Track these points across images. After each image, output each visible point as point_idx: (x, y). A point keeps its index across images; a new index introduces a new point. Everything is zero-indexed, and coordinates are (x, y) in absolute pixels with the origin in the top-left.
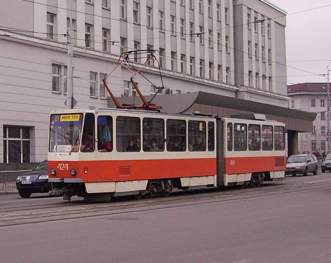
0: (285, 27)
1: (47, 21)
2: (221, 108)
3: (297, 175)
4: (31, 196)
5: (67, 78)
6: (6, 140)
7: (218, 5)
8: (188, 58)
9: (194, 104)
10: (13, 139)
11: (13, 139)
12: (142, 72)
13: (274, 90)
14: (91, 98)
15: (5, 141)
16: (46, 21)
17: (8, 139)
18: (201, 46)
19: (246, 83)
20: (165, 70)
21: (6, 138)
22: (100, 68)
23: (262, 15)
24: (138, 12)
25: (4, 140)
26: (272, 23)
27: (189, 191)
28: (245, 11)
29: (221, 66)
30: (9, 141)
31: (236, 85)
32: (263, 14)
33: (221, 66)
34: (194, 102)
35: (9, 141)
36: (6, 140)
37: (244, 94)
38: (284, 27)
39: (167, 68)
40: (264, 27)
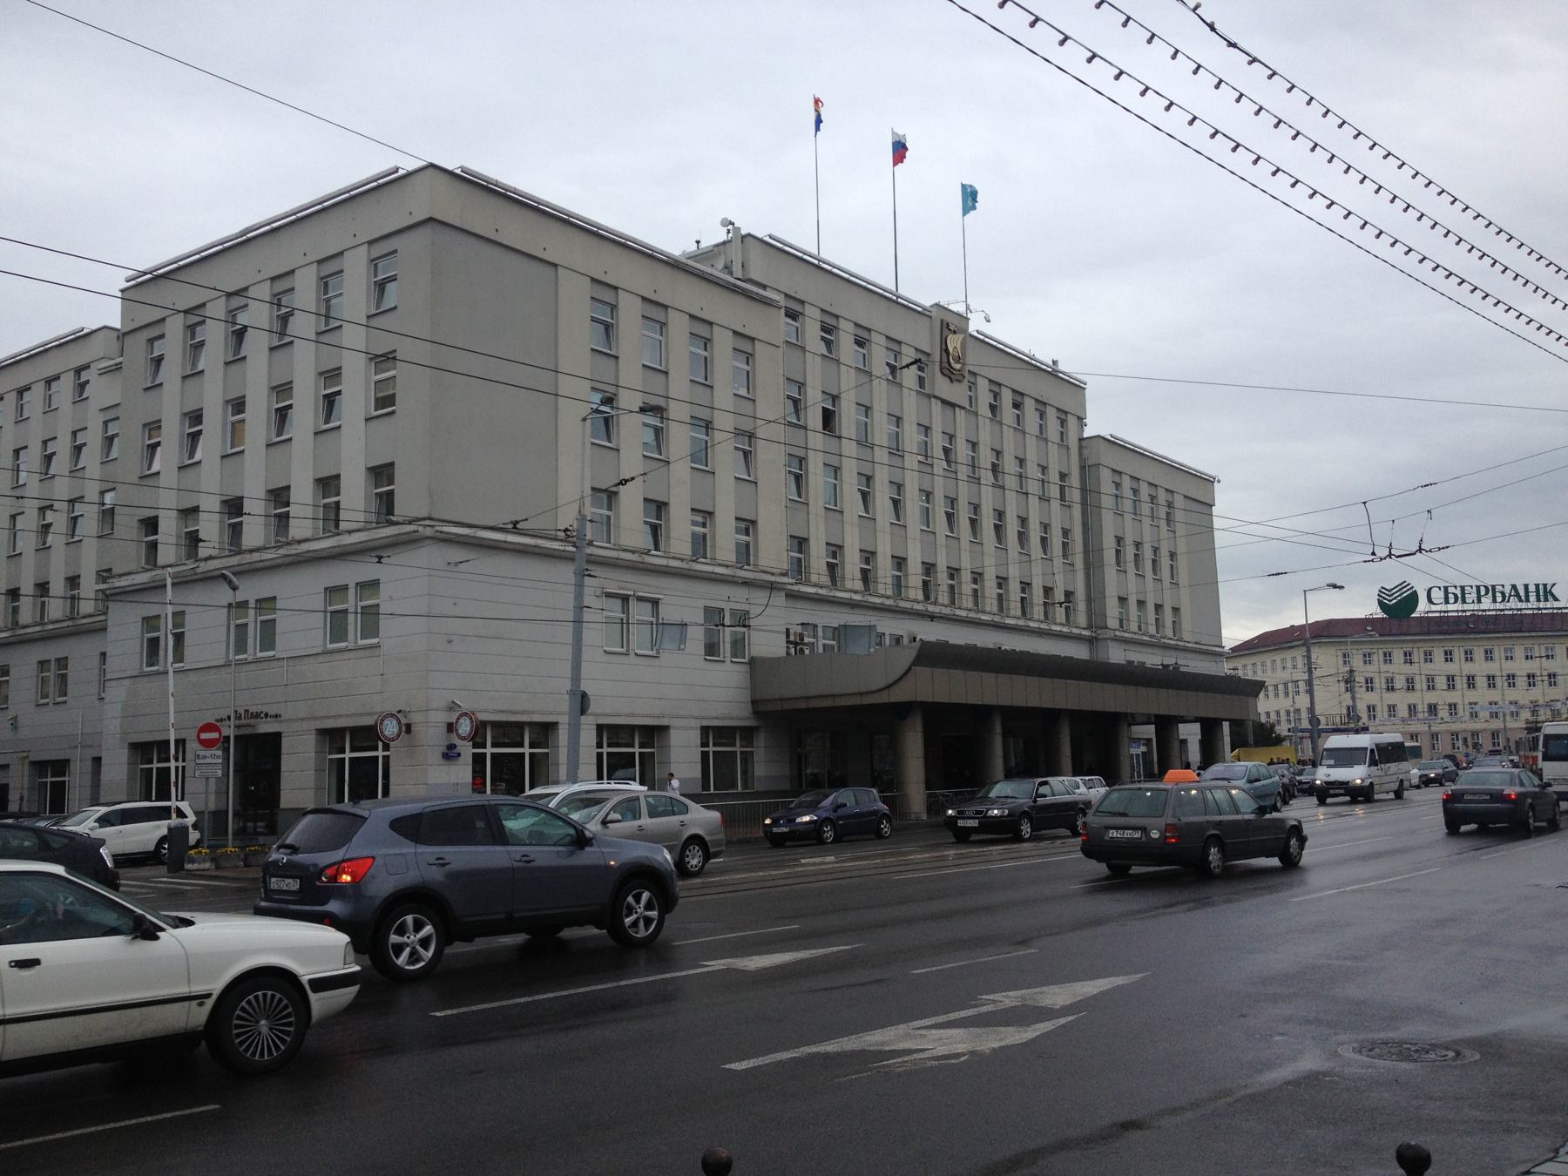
0: (1213, 507)
1: (645, 517)
2: (1063, 680)
3: (1135, 870)
4: (971, 839)
5: (1292, 682)
6: (602, 753)
7: (1042, 466)
8: (966, 577)
9: (913, 668)
10: (745, 749)
11: (745, 749)
12: (376, 551)
13: (1187, 636)
14: (705, 659)
15: (599, 756)
16: (642, 514)
17: (605, 750)
18: (1119, 573)
19: (1112, 623)
20: (908, 600)
21: (602, 747)
22: (730, 599)
23: (1166, 490)
24: (1158, 563)
25: (598, 753)
26: (1179, 501)
27: (196, 999)
28: (1106, 476)
29: (1161, 606)
30: (714, 752)
31: (1089, 627)
32: (1134, 475)
33: (1161, 606)
34: (914, 661)
35: (714, 752)
36: (602, 753)
37: (1108, 647)
38: (1212, 506)
39: (988, 608)
40: (903, 433)
